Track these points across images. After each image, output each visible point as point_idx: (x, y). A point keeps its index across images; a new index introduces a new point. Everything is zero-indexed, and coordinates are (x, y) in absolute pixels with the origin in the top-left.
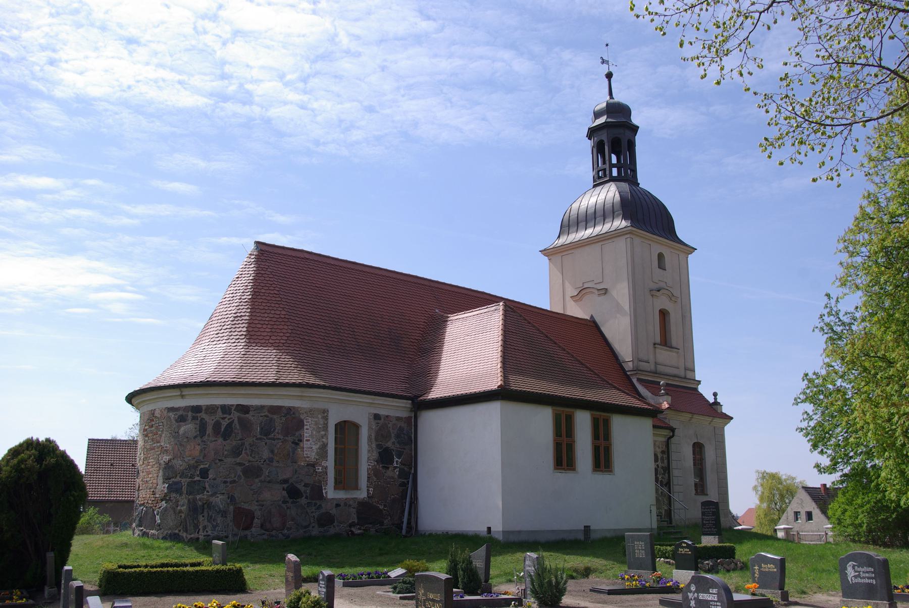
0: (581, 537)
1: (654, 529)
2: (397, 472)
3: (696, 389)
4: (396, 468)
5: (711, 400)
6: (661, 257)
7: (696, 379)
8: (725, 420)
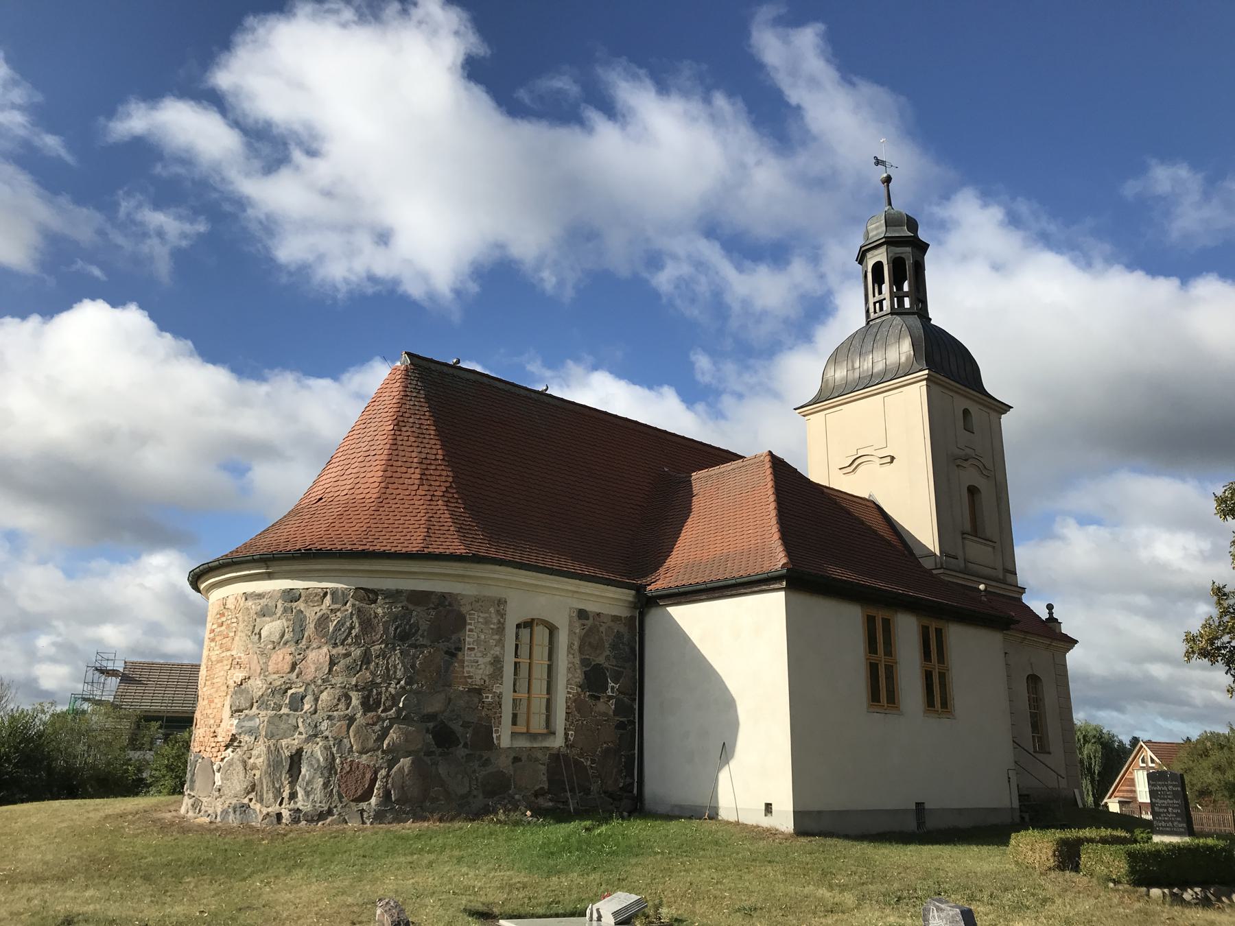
2: (612, 704)
3: (1020, 600)
4: (610, 698)
5: (1044, 615)
6: (966, 412)
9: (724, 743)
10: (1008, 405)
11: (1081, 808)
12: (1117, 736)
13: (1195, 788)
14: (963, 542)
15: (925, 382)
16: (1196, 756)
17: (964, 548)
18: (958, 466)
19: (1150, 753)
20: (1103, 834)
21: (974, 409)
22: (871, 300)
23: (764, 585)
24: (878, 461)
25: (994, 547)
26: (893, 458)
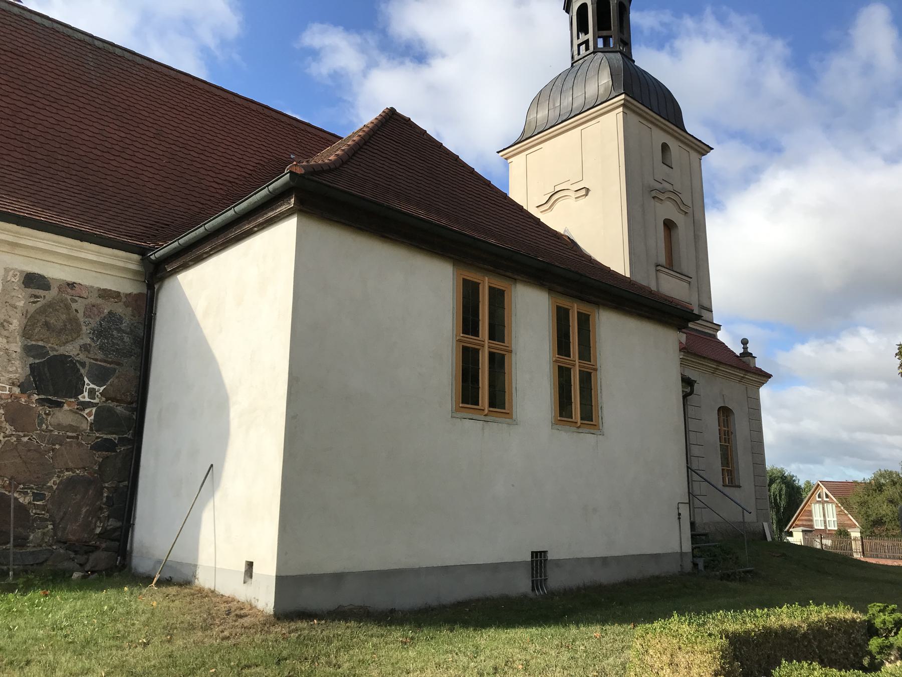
0: (522, 585)
1: (686, 553)
2: (89, 414)
3: (715, 336)
4: (85, 405)
5: (738, 350)
6: (665, 147)
7: (714, 322)
8: (762, 378)
9: (212, 466)
10: (708, 146)
11: (770, 542)
12: (796, 477)
13: (871, 519)
14: (656, 274)
15: (621, 109)
16: (871, 491)
17: (657, 278)
18: (654, 198)
19: (825, 490)
20: (814, 618)
21: (673, 144)
22: (576, 42)
23: (269, 212)
24: (574, 195)
25: (689, 283)
26: (588, 190)
